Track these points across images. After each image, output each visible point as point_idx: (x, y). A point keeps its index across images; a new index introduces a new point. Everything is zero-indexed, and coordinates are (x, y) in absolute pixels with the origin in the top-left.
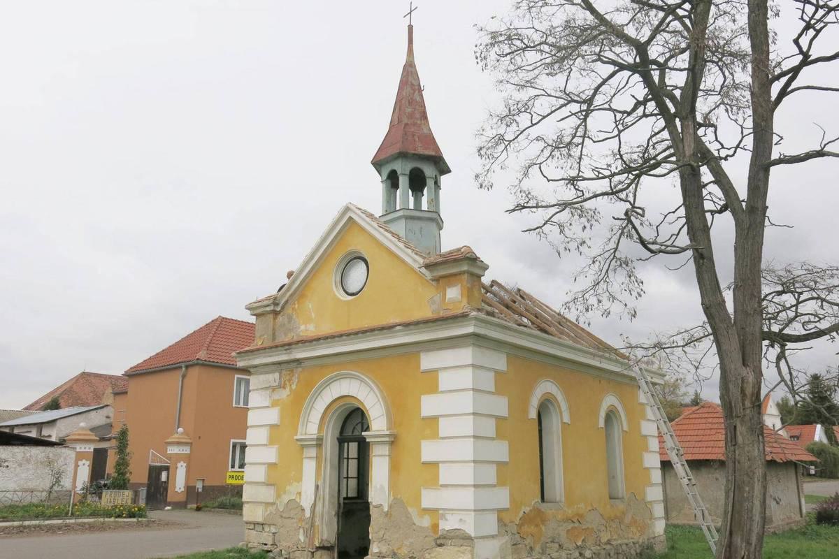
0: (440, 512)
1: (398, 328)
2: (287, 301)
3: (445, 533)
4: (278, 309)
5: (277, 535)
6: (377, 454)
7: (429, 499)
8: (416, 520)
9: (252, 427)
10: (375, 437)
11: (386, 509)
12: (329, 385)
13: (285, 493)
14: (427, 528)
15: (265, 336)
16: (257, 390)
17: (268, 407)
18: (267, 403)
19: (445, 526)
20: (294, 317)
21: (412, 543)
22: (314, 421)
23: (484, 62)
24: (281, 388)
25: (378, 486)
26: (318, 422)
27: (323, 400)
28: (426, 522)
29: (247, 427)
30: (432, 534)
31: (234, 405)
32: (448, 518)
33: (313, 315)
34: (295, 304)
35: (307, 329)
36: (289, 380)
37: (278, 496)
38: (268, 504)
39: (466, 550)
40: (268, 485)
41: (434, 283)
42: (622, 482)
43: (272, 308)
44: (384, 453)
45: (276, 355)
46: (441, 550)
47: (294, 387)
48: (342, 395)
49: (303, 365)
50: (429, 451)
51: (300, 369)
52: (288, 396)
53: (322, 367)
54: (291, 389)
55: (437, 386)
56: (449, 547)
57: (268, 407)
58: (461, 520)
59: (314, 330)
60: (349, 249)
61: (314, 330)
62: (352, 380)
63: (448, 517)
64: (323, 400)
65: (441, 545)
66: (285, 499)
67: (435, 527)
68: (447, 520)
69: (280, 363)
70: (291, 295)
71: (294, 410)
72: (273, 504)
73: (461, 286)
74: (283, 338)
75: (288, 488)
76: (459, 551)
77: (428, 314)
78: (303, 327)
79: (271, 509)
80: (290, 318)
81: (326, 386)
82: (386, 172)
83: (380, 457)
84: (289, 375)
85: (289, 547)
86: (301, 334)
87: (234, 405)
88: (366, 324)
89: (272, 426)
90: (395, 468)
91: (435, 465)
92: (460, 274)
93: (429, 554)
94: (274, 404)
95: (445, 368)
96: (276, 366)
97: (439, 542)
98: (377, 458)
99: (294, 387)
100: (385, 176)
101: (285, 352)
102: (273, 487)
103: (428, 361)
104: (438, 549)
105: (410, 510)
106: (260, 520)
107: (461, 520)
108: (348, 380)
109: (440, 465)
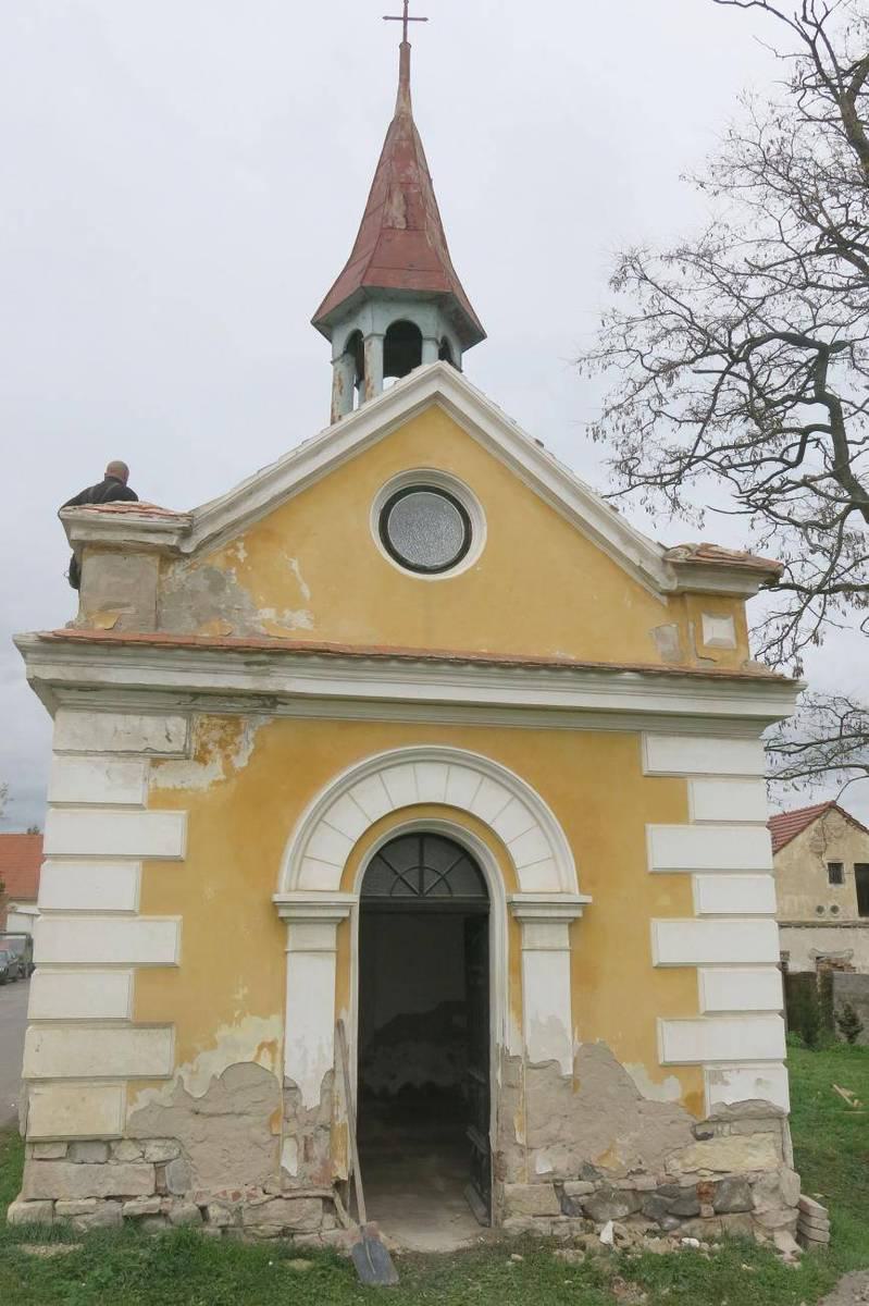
0: (709, 1068)
1: (628, 675)
2: (215, 536)
3: (724, 1110)
4: (187, 548)
5: (169, 1169)
6: (538, 944)
7: (677, 1042)
8: (649, 1091)
9: (56, 857)
10: (550, 908)
11: (568, 1071)
12: (378, 771)
13: (213, 1045)
14: (676, 1103)
15: (130, 611)
16: (86, 753)
17: (138, 807)
18: (138, 795)
19: (720, 1096)
21: (637, 1140)
22: (324, 861)
23: (712, 231)
24: (187, 758)
25: (543, 1020)
26: (342, 860)
27: (508, 804)
28: (671, 1091)
29: (43, 858)
30: (687, 1117)
32: (730, 1080)
34: (237, 550)
35: (268, 620)
36: (222, 744)
37: (184, 1056)
38: (136, 1082)
39: (765, 1139)
40: (140, 1026)
41: (664, 599)
42: (503, 994)
43: (173, 541)
44: (557, 945)
45: (206, 671)
46: (708, 1148)
47: (241, 762)
48: (422, 801)
49: (280, 709)
50: (671, 941)
51: (263, 720)
52: (217, 783)
53: (345, 724)
54: (228, 769)
55: (687, 812)
56: (722, 1140)
57: (138, 807)
58: (759, 1081)
59: (308, 626)
60: (425, 463)
61: (308, 626)
62: (454, 769)
63: (727, 1076)
64: (508, 804)
65: (705, 1137)
66: (215, 1063)
67: (694, 1101)
68: (726, 1083)
69: (196, 694)
70: (234, 525)
71: (256, 820)
72: (166, 1079)
73: (735, 621)
74: (184, 628)
75: (224, 1032)
76: (747, 1145)
77: (653, 657)
79: (162, 1095)
80: (217, 583)
81: (374, 773)
82: (342, 336)
83: (546, 954)
84: (223, 728)
85: (237, 1195)
86: (262, 629)
88: (483, 646)
89: (151, 863)
90: (583, 976)
91: (689, 970)
92: (731, 597)
93: (680, 1158)
94: (160, 800)
95: (706, 775)
96: (178, 698)
97: (700, 1131)
98: (304, 959)
99: (241, 762)
100: (341, 348)
101: (243, 667)
102: (168, 1031)
103: (662, 755)
104: (699, 1145)
105: (628, 1067)
106: (113, 1128)
107: (759, 1081)
108: (440, 769)
109: (701, 970)
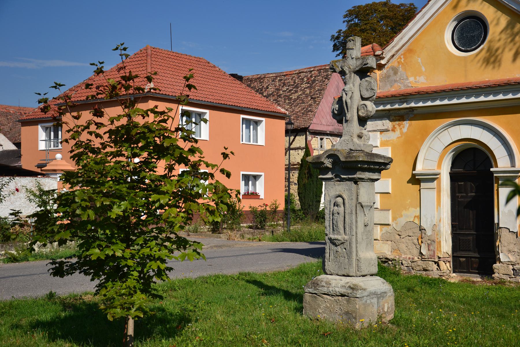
20: (401, 69)
31: (241, 142)
33: (423, 69)
34: (401, 59)
54: (401, 133)
78: (411, 79)
86: (410, 85)
87: (241, 142)
99: (405, 130)
